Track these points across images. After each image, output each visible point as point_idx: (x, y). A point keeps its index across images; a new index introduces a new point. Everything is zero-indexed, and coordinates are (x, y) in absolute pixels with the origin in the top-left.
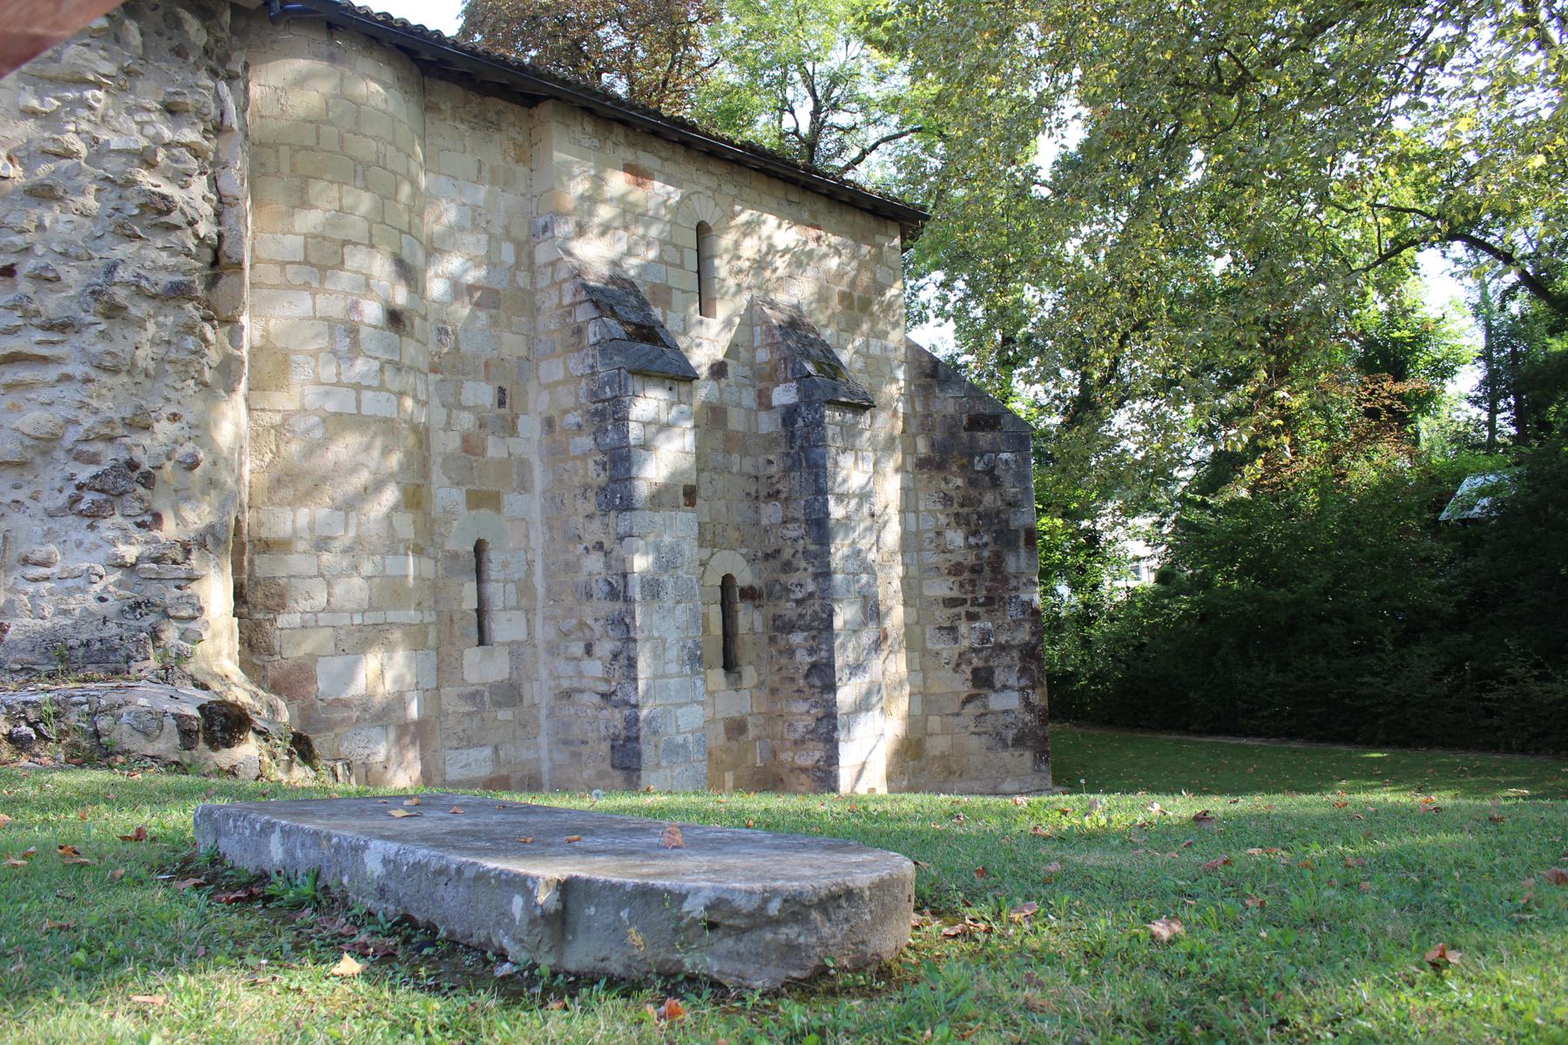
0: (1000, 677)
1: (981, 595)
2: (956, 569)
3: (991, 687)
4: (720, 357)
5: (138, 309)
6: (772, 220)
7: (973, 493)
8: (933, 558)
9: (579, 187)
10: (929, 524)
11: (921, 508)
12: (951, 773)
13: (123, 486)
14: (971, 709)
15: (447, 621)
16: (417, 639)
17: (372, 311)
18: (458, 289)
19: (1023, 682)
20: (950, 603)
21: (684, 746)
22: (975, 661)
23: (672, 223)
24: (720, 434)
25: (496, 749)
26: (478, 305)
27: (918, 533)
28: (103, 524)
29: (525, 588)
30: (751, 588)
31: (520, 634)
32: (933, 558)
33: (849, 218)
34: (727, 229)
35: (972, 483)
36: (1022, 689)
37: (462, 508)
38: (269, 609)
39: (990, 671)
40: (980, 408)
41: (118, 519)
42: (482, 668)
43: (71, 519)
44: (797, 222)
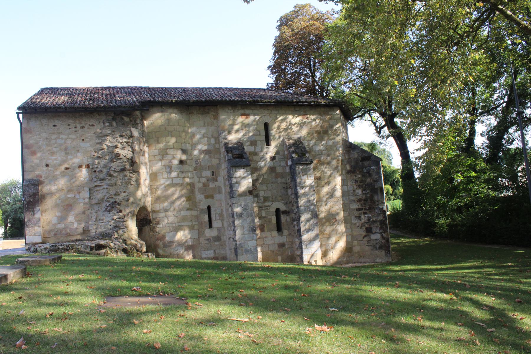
0: (374, 230)
1: (367, 207)
2: (360, 200)
3: (372, 232)
4: (273, 155)
5: (115, 174)
6: (290, 117)
7: (364, 179)
8: (352, 198)
9: (229, 122)
10: (351, 188)
11: (349, 184)
12: (361, 256)
13: (113, 206)
14: (366, 239)
15: (201, 224)
16: (191, 228)
17: (176, 162)
18: (201, 152)
19: (381, 231)
20: (358, 210)
21: (251, 250)
22: (366, 225)
23: (257, 125)
24: (274, 174)
25: (215, 251)
26: (206, 154)
27: (348, 191)
28: (111, 213)
29: (221, 215)
30: (286, 211)
31: (220, 225)
32: (352, 198)
33: (319, 110)
34: (275, 123)
35: (363, 176)
36: (381, 233)
37: (204, 199)
38: (156, 224)
39: (371, 228)
40: (365, 155)
41: (113, 212)
42: (210, 233)
43: (106, 212)
44: (299, 115)
